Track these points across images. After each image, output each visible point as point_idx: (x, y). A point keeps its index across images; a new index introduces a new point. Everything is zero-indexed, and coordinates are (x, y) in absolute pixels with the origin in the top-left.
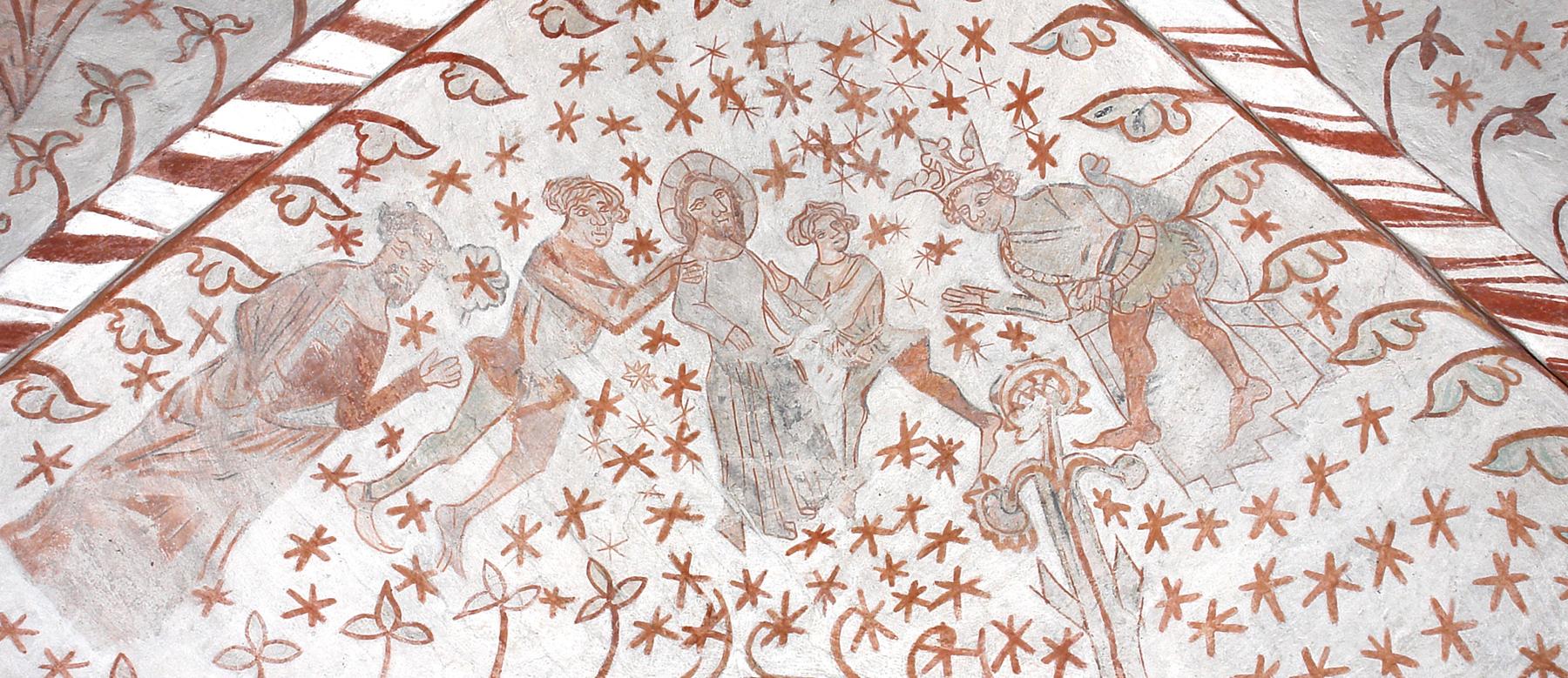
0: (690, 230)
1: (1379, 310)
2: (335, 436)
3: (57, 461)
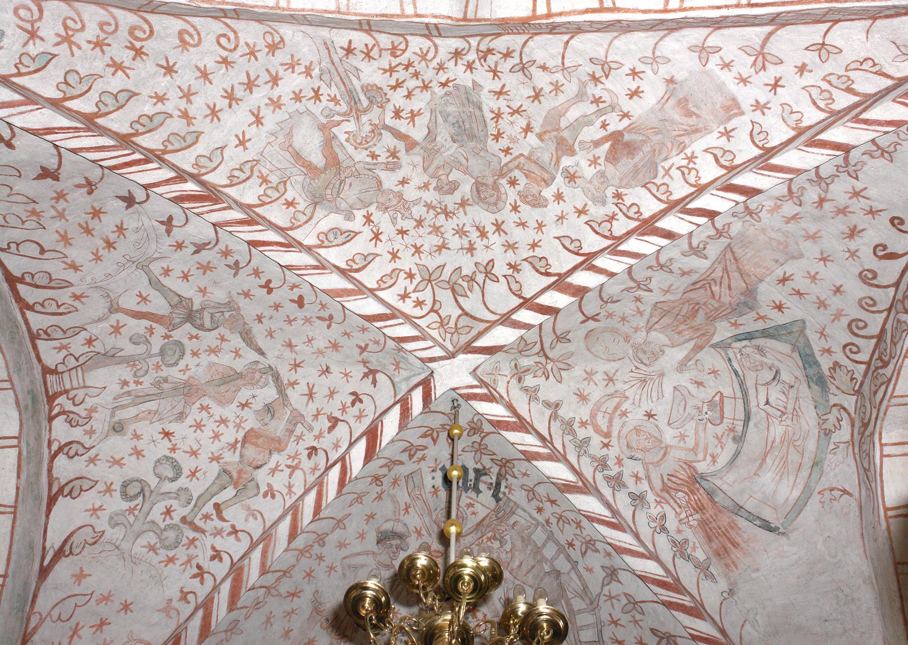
0: (496, 187)
1: (244, 181)
2: (625, 129)
3: (722, 134)
